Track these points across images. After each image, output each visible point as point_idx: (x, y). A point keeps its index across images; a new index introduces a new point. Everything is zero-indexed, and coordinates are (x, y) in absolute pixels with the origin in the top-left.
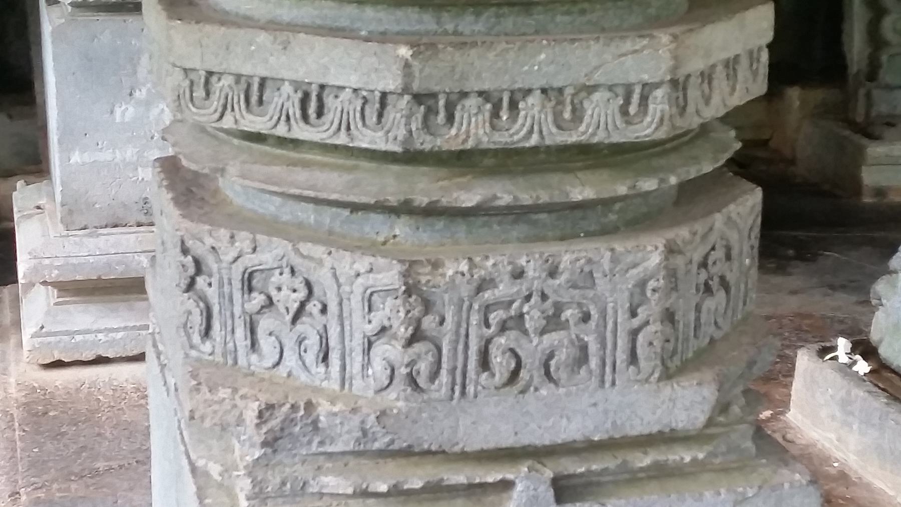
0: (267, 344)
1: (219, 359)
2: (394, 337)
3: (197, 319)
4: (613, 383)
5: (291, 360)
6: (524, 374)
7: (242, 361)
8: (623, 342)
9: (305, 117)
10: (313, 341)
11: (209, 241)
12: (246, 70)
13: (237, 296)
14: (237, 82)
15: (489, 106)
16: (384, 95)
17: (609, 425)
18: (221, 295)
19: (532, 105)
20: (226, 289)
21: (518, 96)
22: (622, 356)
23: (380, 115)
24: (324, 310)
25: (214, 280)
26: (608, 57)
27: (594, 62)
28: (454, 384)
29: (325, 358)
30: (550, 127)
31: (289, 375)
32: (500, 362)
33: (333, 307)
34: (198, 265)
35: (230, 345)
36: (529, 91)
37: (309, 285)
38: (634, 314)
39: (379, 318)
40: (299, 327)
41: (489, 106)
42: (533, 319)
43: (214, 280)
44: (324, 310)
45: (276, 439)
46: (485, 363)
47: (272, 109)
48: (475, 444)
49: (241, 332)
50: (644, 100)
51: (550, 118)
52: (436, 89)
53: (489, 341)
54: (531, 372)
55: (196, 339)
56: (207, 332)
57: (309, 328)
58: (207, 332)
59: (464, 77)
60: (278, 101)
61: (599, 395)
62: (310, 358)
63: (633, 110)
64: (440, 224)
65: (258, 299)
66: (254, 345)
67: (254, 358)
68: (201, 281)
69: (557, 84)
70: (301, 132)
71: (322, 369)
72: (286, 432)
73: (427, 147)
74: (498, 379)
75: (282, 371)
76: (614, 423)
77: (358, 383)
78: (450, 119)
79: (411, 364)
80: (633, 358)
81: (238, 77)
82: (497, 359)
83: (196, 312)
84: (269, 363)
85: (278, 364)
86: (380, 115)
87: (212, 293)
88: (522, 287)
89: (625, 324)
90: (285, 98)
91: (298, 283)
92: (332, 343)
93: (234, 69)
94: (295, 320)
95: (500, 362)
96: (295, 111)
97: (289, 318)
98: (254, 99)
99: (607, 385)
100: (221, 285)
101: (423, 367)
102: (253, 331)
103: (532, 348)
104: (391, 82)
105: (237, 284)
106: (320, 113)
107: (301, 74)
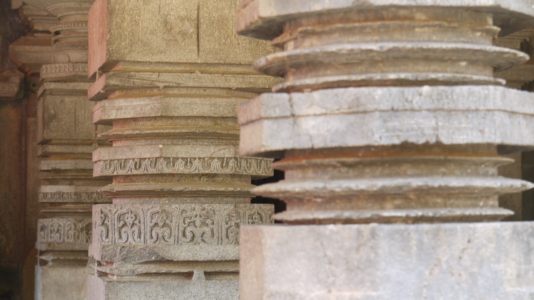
0: (124, 236)
1: (110, 243)
2: (158, 226)
3: (104, 232)
4: (221, 244)
5: (130, 239)
6: (196, 239)
7: (117, 242)
8: (224, 232)
9: (136, 168)
10: (137, 231)
11: (109, 208)
12: (120, 157)
13: (116, 222)
14: (118, 162)
15: (184, 162)
16: (156, 158)
17: (220, 256)
18: (112, 224)
19: (196, 163)
20: (113, 222)
21: (192, 160)
22: (224, 236)
23: (155, 165)
24: (140, 222)
25: (110, 220)
26: (216, 150)
27: (212, 151)
28: (175, 240)
29: (140, 237)
30: (201, 169)
31: (130, 243)
32: (189, 235)
33: (142, 220)
34: (106, 216)
35: (114, 238)
36: (195, 159)
37: (136, 215)
38: (227, 224)
39: (154, 221)
40: (133, 229)
41: (184, 162)
42: (198, 223)
43: (110, 220)
44: (140, 222)
45: (125, 258)
46: (184, 235)
47: (127, 168)
48: (181, 258)
49: (117, 234)
50: (227, 163)
51: (201, 166)
52: (170, 156)
53: (185, 228)
54: (198, 239)
55: (104, 238)
56: (107, 237)
57: (136, 228)
58: (107, 237)
59: (177, 153)
60: (128, 165)
61: (217, 247)
62: (136, 237)
63: (224, 165)
64: (164, 120)
65: (122, 223)
66: (120, 237)
67: (120, 241)
68: (106, 222)
69: (202, 156)
70: (135, 172)
71: (139, 239)
72: (128, 256)
73: (167, 172)
74: (188, 240)
75: (128, 243)
76: (222, 256)
77: (149, 241)
78: (174, 165)
79: (163, 233)
80: (227, 237)
81: (119, 160)
82: (188, 234)
83: (104, 230)
84: (124, 241)
85: (127, 241)
86: (155, 165)
87: (109, 224)
88: (195, 213)
89: (225, 227)
90: (131, 164)
91: (133, 216)
92: (142, 231)
93: (117, 158)
94: (131, 227)
95: (189, 235)
96: (133, 167)
97: (130, 226)
98: (122, 166)
99: (220, 244)
100: (112, 221)
101: (166, 234)
102: (120, 233)
103: (198, 232)
104: (157, 155)
105: (116, 219)
106: (140, 167)
107: (135, 156)
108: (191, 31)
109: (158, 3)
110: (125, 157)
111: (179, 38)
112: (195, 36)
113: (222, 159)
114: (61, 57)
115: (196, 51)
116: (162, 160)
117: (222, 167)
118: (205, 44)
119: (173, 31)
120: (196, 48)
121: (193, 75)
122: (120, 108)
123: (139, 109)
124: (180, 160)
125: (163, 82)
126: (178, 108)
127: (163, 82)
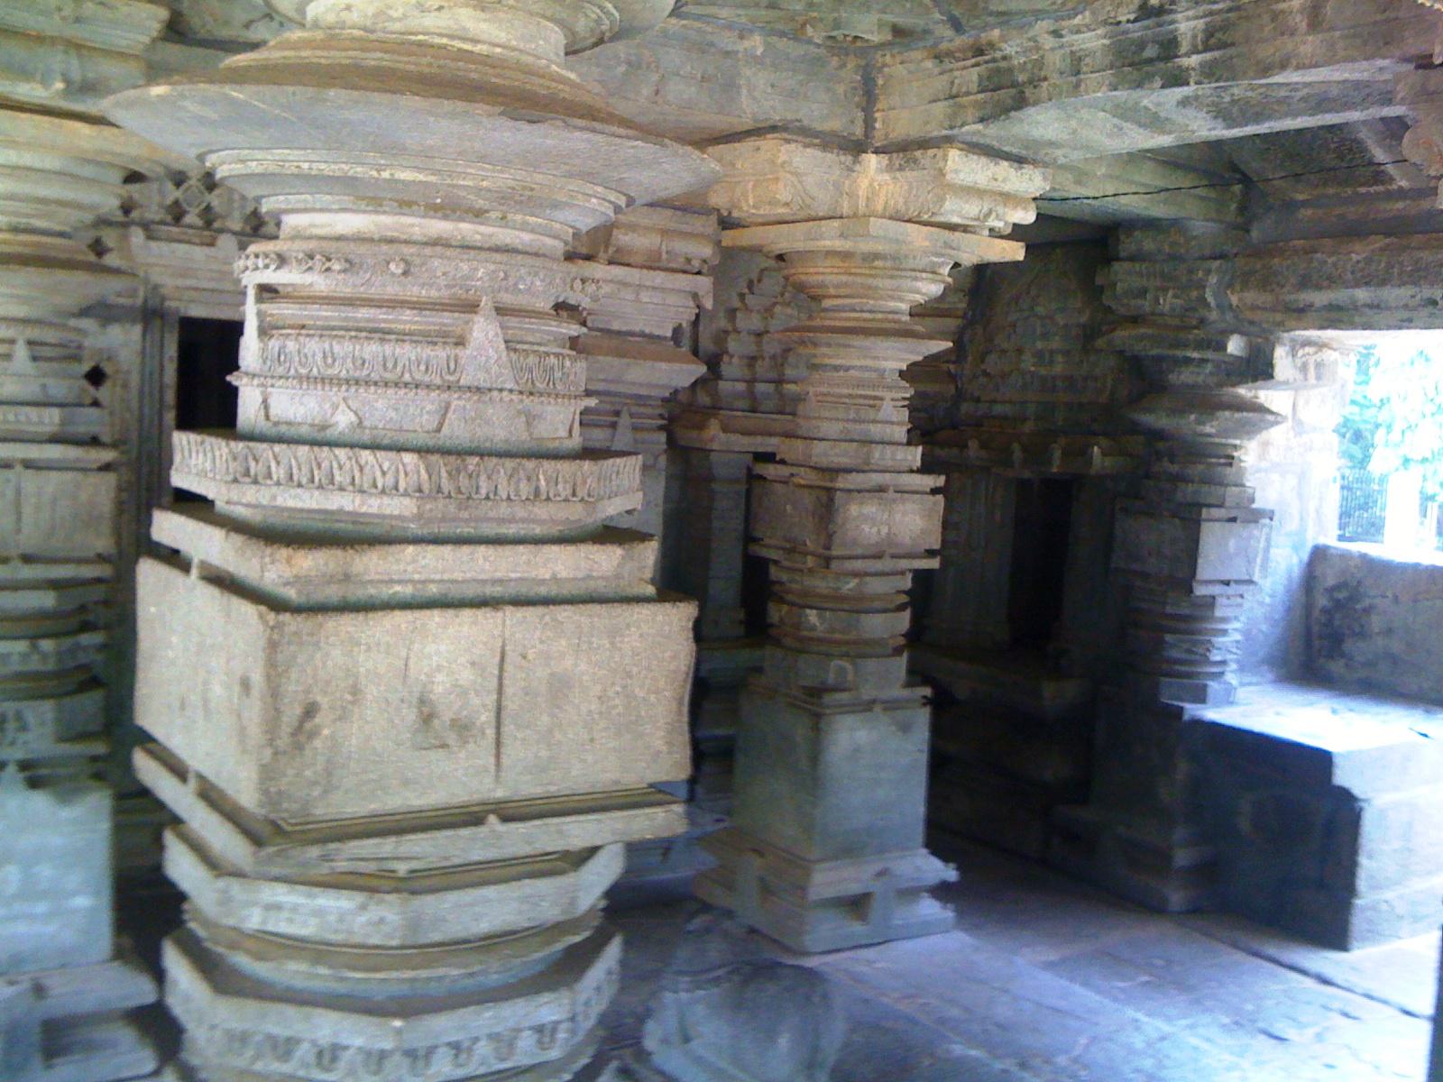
96: (311, 1058)
108: (483, 718)
109: (404, 653)
110: (287, 1033)
111: (451, 739)
112: (491, 732)
113: (539, 1029)
114: (744, 20)
115: (492, 768)
116: (397, 1058)
117: (456, 356)
118: (512, 752)
119: (436, 722)
120: (492, 760)
121: (482, 831)
122: (278, 907)
123: (332, 918)
124: (442, 1050)
125: (407, 858)
126: (444, 920)
127: (407, 858)
